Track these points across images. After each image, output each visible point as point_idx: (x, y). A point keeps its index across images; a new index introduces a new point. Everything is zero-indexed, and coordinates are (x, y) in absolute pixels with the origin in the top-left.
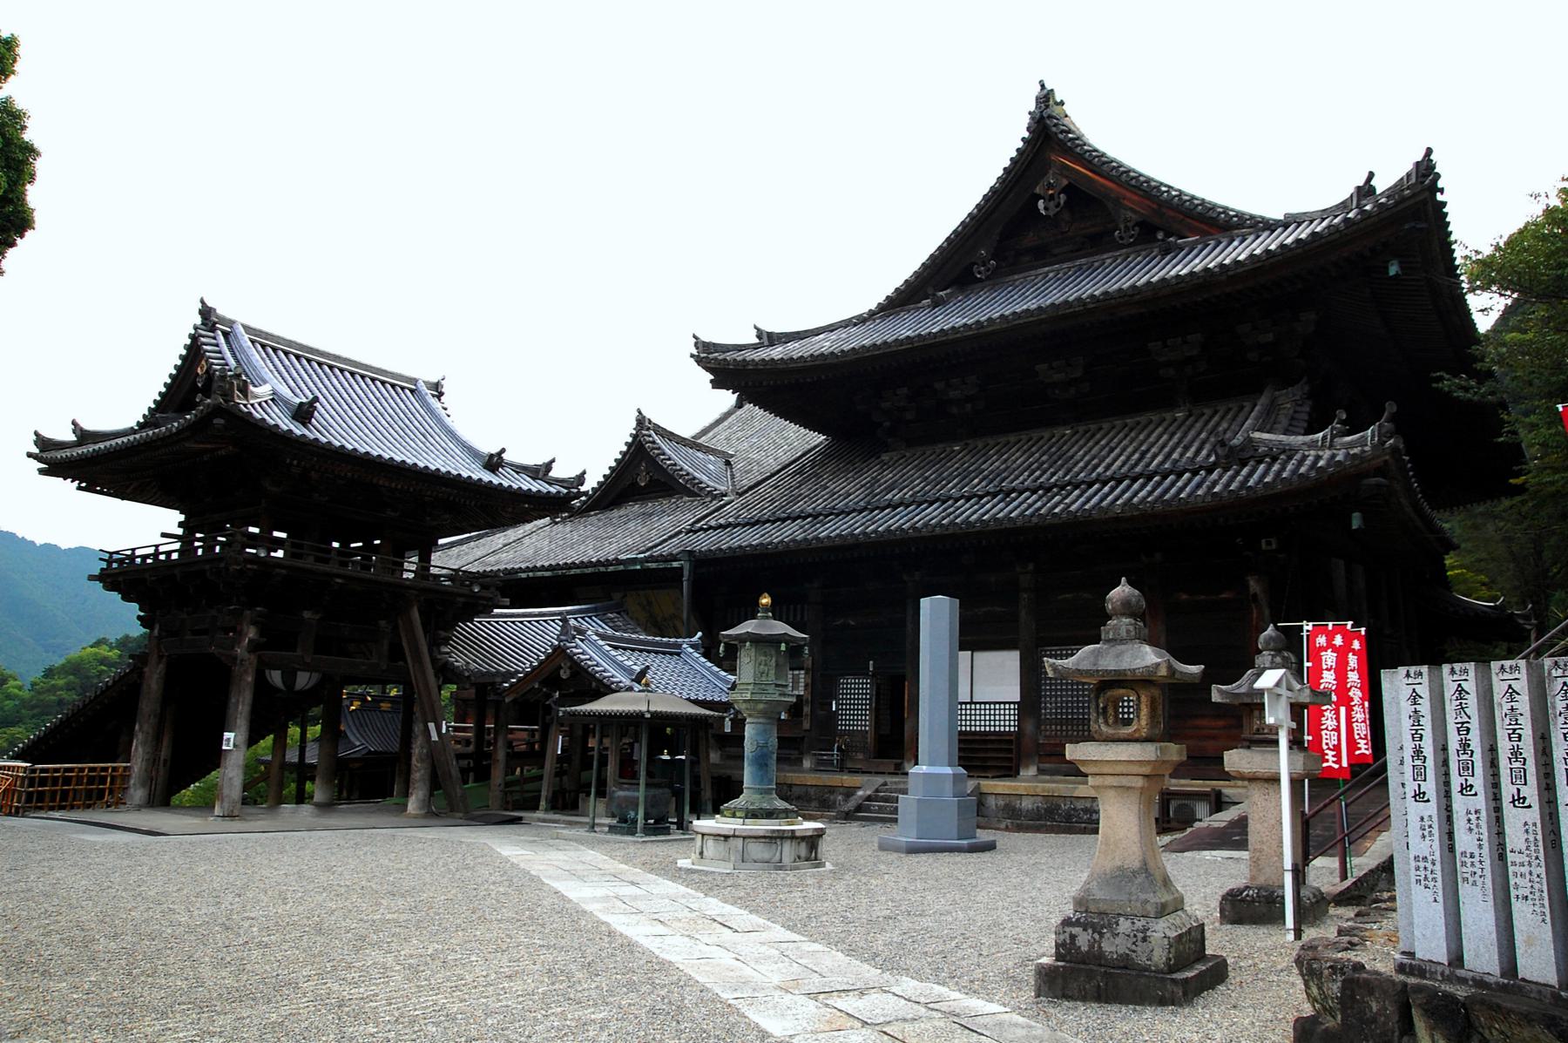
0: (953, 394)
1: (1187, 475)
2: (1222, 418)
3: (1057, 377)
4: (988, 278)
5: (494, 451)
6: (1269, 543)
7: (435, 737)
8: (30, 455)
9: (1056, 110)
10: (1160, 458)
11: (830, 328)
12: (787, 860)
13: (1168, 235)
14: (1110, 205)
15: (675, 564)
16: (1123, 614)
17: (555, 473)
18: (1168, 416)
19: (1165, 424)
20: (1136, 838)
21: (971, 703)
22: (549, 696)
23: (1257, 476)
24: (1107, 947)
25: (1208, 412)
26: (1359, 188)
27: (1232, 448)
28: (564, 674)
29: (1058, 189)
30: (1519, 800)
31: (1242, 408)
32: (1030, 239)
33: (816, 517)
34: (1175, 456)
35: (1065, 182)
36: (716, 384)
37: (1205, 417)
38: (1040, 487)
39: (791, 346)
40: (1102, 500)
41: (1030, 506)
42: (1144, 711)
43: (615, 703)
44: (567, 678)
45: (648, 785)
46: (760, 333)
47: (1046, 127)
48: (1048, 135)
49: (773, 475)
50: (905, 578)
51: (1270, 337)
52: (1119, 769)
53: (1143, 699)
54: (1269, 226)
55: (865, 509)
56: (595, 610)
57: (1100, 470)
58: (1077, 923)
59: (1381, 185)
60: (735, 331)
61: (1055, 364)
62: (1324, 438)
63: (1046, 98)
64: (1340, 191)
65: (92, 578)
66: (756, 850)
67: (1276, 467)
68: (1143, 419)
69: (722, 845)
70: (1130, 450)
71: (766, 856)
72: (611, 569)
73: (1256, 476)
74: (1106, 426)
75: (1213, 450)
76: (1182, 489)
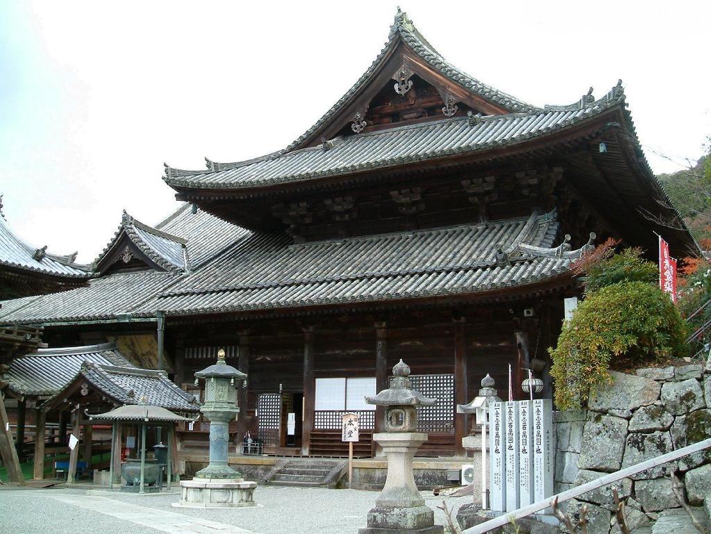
0: (338, 208)
1: (480, 270)
2: (506, 231)
3: (404, 200)
4: (361, 132)
5: (40, 248)
6: (528, 312)
9: (408, 27)
10: (465, 258)
11: (257, 161)
12: (236, 501)
13: (475, 112)
14: (440, 90)
16: (400, 376)
17: (78, 261)
18: (473, 228)
19: (471, 234)
20: (403, 474)
21: (345, 411)
22: (73, 407)
23: (520, 274)
24: (389, 520)
25: (498, 226)
26: (584, 97)
27: (505, 255)
28: (84, 392)
29: (408, 77)
30: (524, 451)
31: (518, 225)
32: (390, 107)
33: (246, 290)
34: (474, 256)
35: (412, 73)
36: (178, 197)
37: (495, 230)
38: (390, 275)
39: (232, 173)
40: (427, 285)
41: (382, 288)
42: (407, 419)
43: (125, 412)
44: (87, 396)
45: (146, 462)
46: (209, 164)
47: (400, 37)
48: (401, 44)
49: (216, 257)
50: (304, 330)
51: (535, 181)
52: (396, 444)
53: (407, 414)
54: (536, 112)
55: (278, 285)
56: (98, 349)
57: (428, 264)
58: (377, 511)
59: (598, 96)
60: (192, 162)
61: (403, 191)
62: (558, 251)
63: (400, 19)
64: (575, 97)
66: (218, 496)
67: (530, 268)
68: (458, 229)
69: (198, 494)
70: (447, 251)
71: (224, 499)
72: (108, 322)
73: (518, 274)
74: (434, 233)
75: (495, 256)
76: (475, 280)
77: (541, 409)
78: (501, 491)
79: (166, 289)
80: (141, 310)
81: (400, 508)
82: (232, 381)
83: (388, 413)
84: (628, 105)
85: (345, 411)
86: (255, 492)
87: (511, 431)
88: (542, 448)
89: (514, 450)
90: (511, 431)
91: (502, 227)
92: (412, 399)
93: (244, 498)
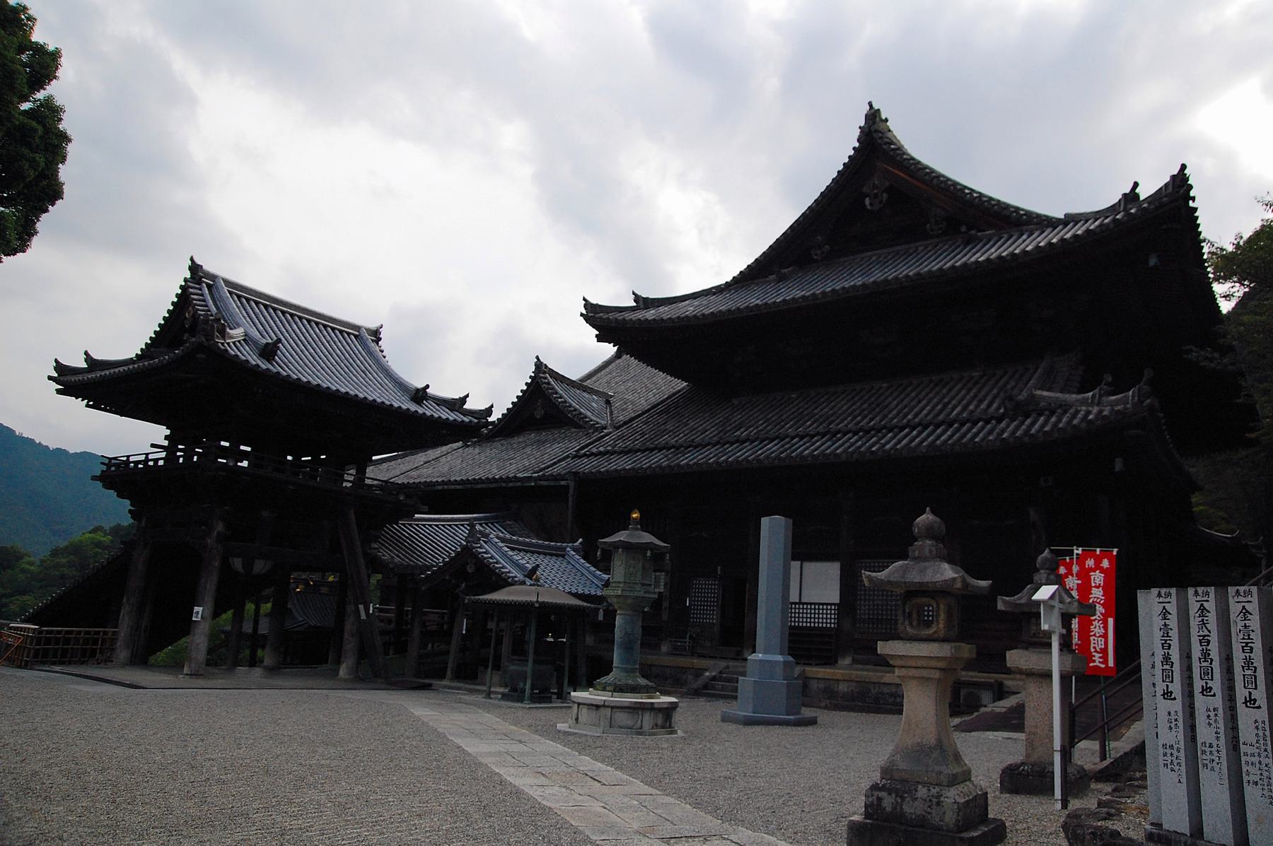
7: (363, 616)
8: (50, 378)
10: (959, 408)
12: (646, 727)
15: (563, 483)
21: (800, 603)
24: (907, 809)
28: (470, 569)
34: (971, 407)
35: (887, 184)
38: (861, 430)
39: (662, 309)
40: (911, 441)
41: (852, 445)
42: (942, 616)
45: (535, 662)
46: (637, 298)
48: (875, 139)
49: (644, 413)
52: (919, 663)
53: (942, 607)
55: (718, 443)
58: (883, 788)
59: (1144, 192)
60: (616, 295)
63: (873, 116)
65: (94, 478)
66: (621, 718)
67: (1053, 419)
70: (935, 400)
71: (630, 723)
77: (1253, 607)
78: (1184, 786)
79: (583, 448)
80: (549, 472)
81: (927, 785)
82: (649, 553)
83: (904, 605)
84: (1193, 199)
85: (800, 603)
86: (677, 717)
87: (1206, 655)
88: (1260, 695)
89: (1219, 695)
90: (1206, 655)
91: (1006, 373)
92: (954, 579)
93: (660, 722)
